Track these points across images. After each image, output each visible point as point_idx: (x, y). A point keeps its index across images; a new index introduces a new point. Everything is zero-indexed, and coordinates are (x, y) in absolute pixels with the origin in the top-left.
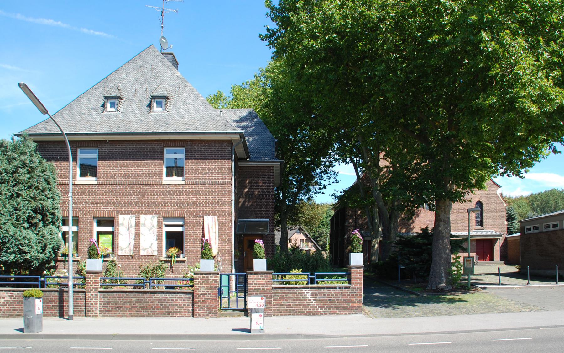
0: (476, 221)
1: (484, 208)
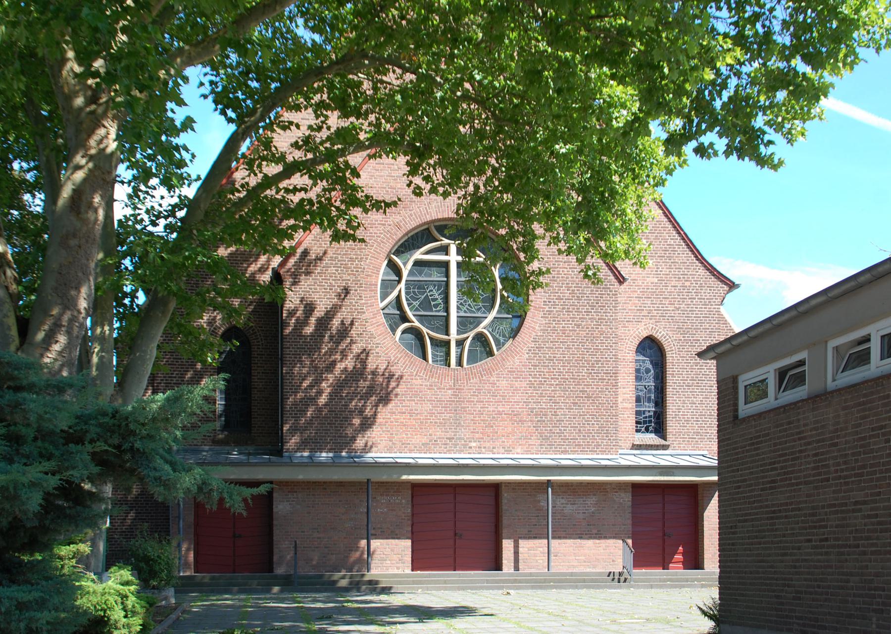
0: (638, 413)
1: (669, 366)
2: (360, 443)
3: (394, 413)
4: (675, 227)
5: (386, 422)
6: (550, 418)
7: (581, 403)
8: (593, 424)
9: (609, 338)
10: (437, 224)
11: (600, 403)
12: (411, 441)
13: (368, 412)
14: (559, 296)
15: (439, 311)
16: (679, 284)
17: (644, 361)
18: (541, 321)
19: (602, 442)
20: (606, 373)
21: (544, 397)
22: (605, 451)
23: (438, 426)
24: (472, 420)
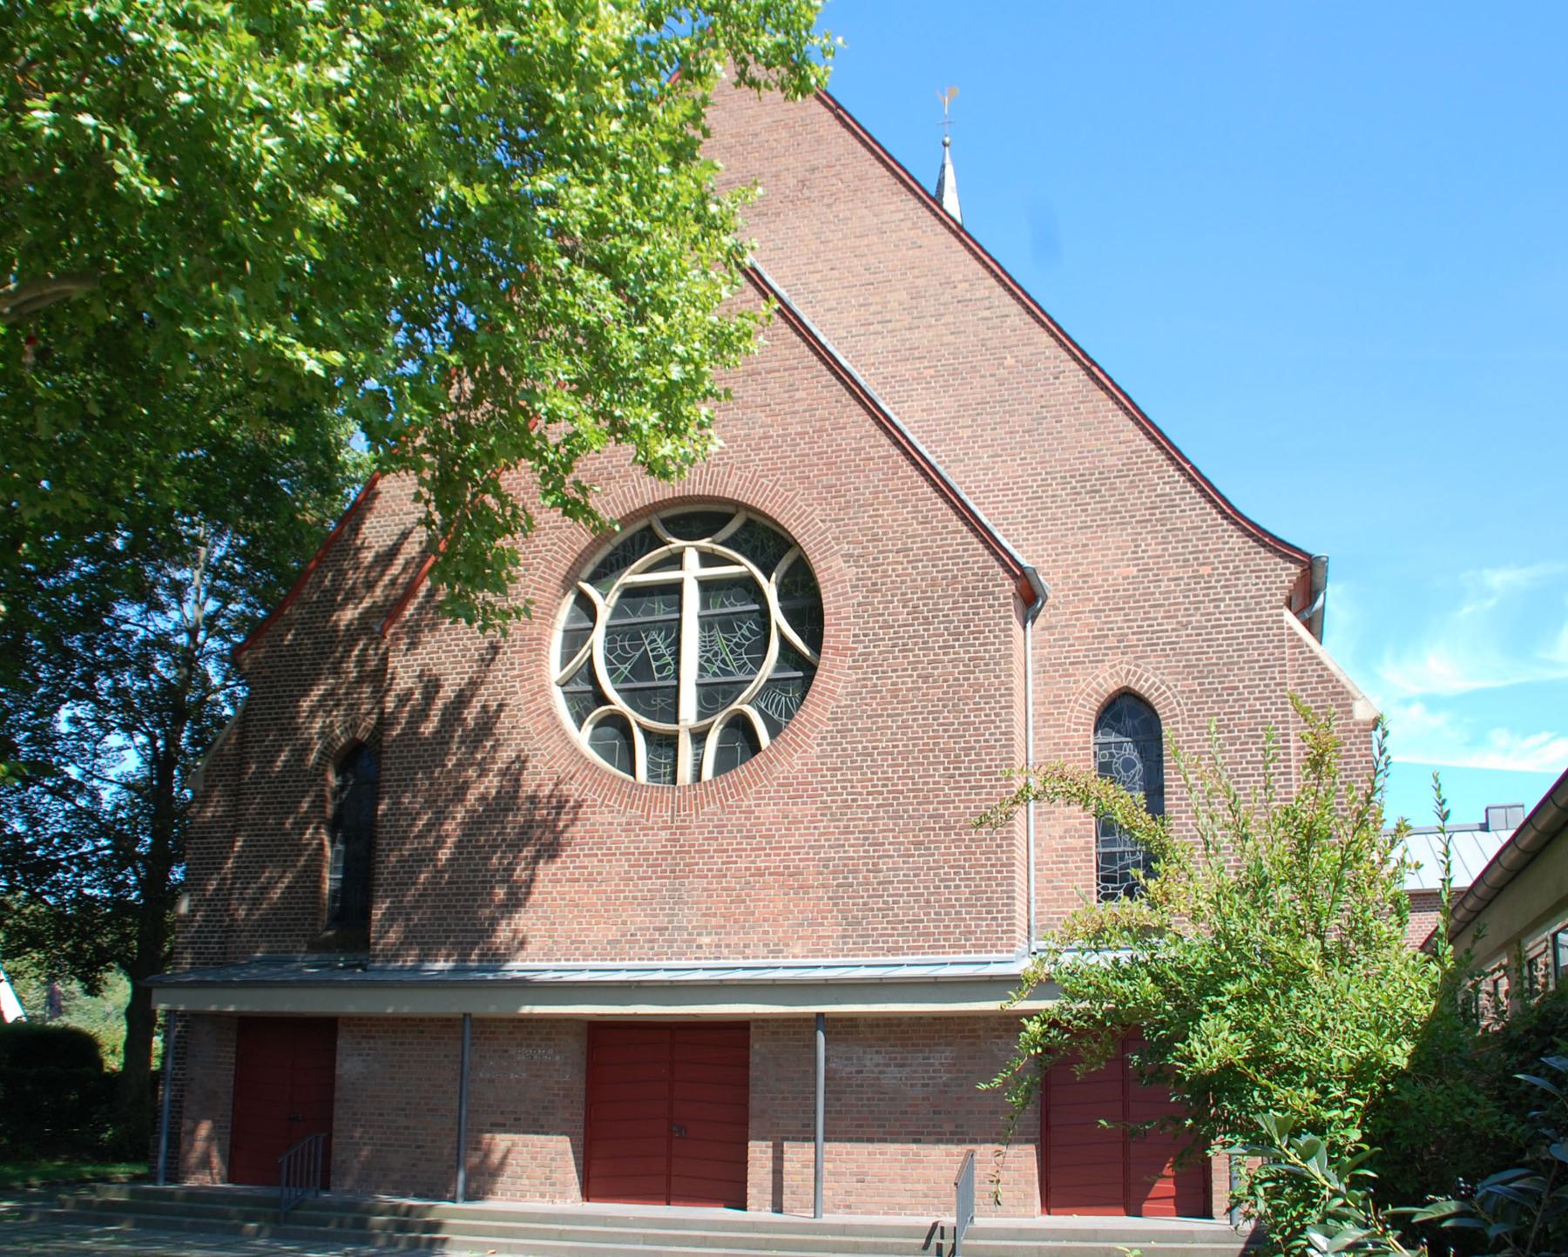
2: (503, 934)
3: (559, 881)
4: (1172, 458)
5: (545, 900)
6: (865, 877)
7: (931, 842)
8: (957, 887)
9: (993, 696)
10: (666, 514)
11: (972, 840)
12: (587, 936)
13: (520, 873)
14: (885, 621)
15: (665, 678)
16: (1186, 574)
17: (1119, 746)
18: (849, 675)
19: (977, 926)
20: (985, 774)
21: (853, 833)
22: (985, 946)
23: (639, 904)
24: (705, 890)
